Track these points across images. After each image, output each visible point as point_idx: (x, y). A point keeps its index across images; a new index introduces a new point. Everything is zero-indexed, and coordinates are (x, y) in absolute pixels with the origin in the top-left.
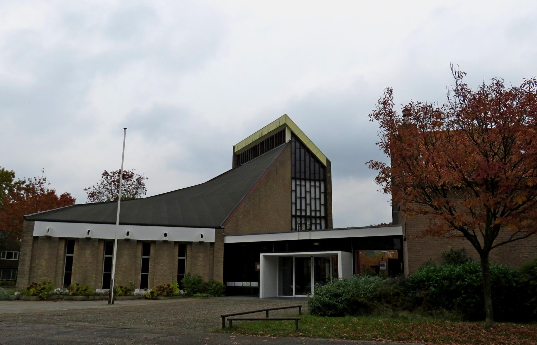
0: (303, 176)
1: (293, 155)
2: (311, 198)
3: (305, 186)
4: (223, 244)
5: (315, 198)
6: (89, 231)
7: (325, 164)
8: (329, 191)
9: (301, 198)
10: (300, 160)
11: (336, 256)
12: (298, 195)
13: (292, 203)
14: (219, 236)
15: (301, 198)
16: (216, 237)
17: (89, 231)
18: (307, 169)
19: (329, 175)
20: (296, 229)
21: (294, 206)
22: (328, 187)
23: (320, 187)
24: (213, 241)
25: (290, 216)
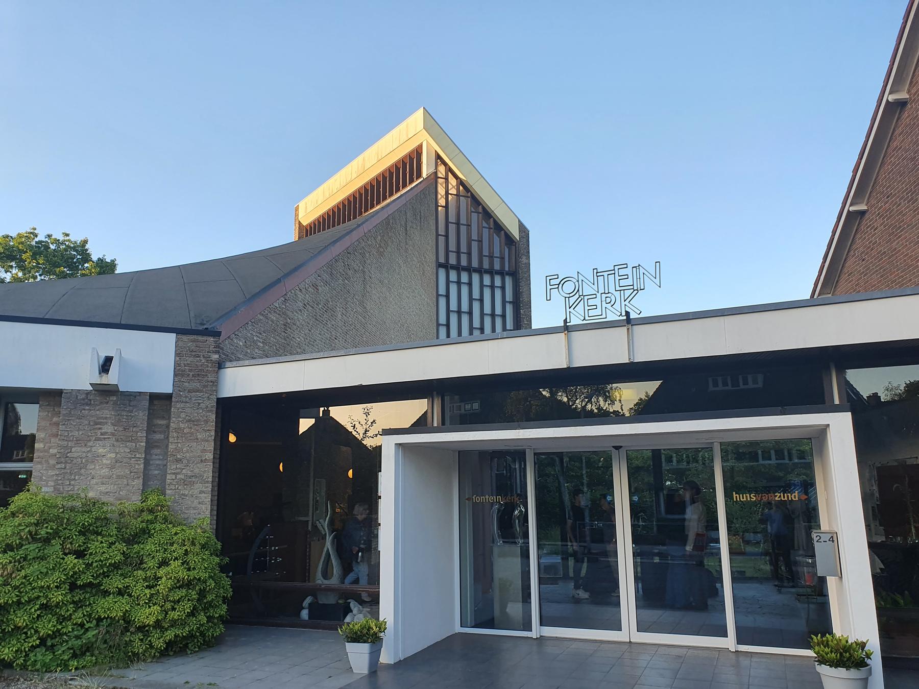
0: (464, 263)
1: (442, 239)
2: (482, 315)
3: (470, 284)
4: (214, 398)
5: (493, 315)
6: (108, 360)
7: (516, 233)
8: (524, 298)
9: (459, 312)
10: (458, 224)
11: (667, 512)
12: (454, 306)
13: (438, 325)
14: (197, 370)
15: (459, 312)
16: (178, 373)
17: (108, 360)
18: (475, 246)
19: (524, 260)
20: (482, 329)
21: (442, 301)
22: (523, 289)
23: (503, 288)
24: (165, 386)
25: (434, 265)
